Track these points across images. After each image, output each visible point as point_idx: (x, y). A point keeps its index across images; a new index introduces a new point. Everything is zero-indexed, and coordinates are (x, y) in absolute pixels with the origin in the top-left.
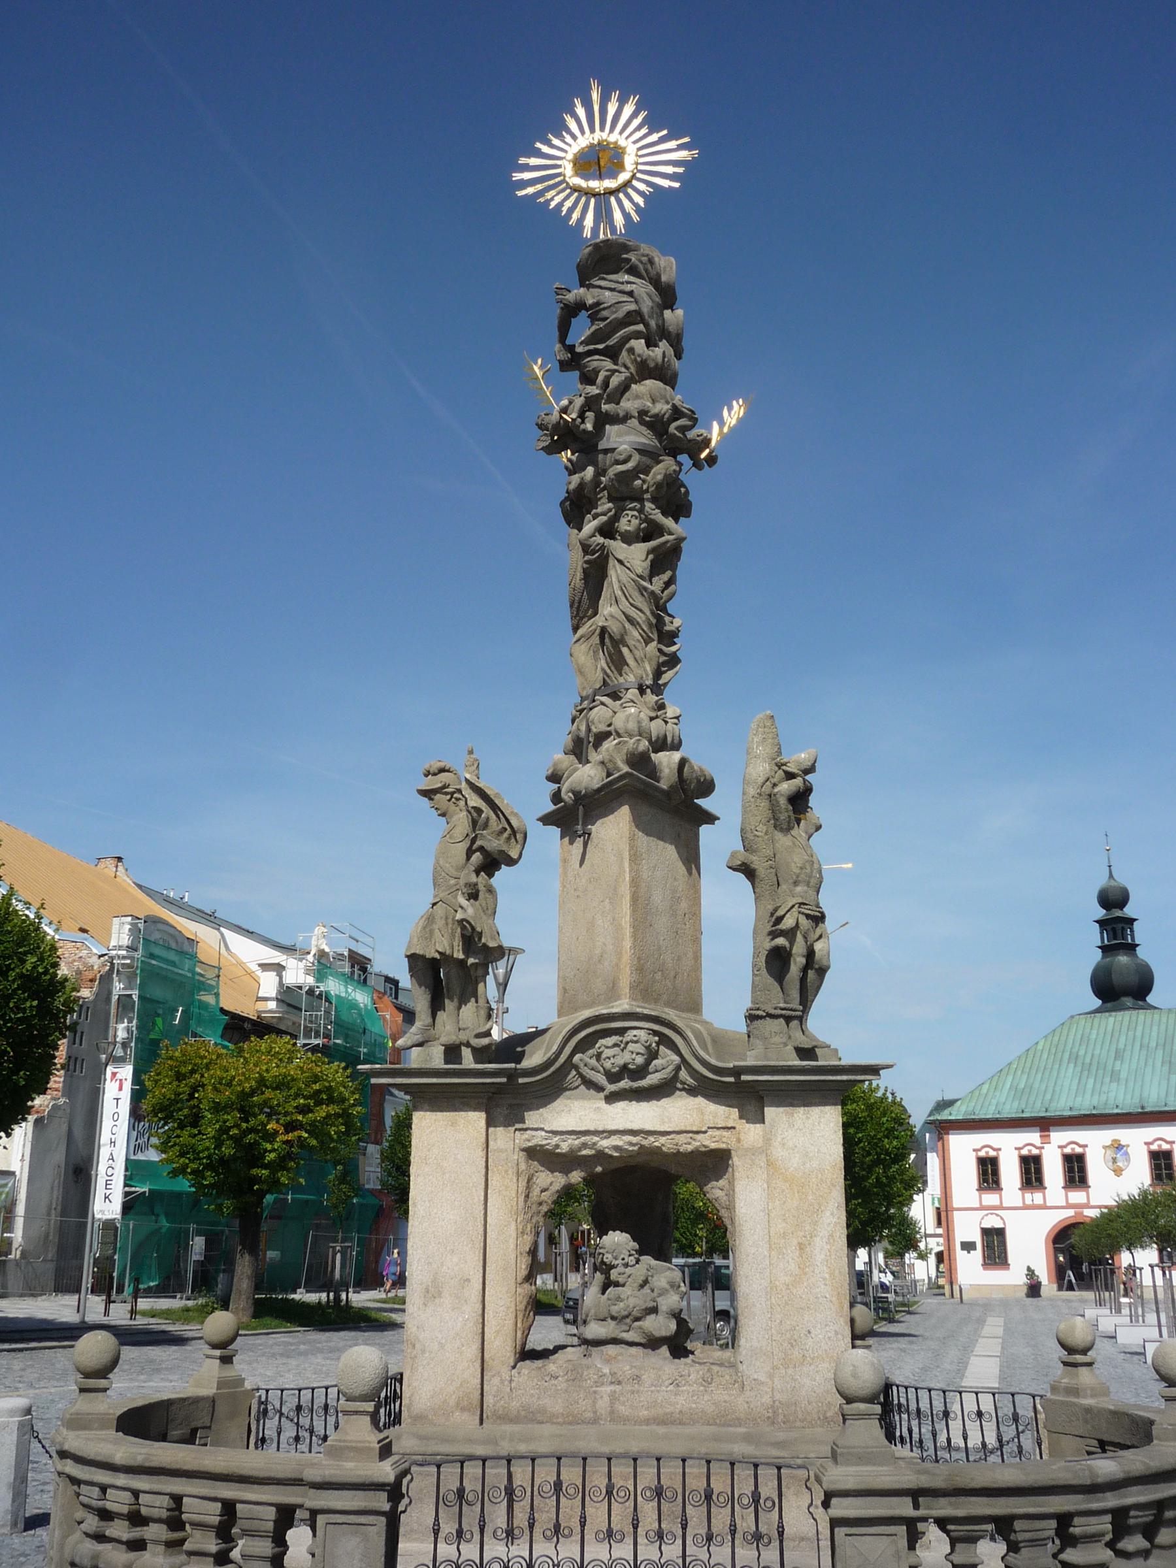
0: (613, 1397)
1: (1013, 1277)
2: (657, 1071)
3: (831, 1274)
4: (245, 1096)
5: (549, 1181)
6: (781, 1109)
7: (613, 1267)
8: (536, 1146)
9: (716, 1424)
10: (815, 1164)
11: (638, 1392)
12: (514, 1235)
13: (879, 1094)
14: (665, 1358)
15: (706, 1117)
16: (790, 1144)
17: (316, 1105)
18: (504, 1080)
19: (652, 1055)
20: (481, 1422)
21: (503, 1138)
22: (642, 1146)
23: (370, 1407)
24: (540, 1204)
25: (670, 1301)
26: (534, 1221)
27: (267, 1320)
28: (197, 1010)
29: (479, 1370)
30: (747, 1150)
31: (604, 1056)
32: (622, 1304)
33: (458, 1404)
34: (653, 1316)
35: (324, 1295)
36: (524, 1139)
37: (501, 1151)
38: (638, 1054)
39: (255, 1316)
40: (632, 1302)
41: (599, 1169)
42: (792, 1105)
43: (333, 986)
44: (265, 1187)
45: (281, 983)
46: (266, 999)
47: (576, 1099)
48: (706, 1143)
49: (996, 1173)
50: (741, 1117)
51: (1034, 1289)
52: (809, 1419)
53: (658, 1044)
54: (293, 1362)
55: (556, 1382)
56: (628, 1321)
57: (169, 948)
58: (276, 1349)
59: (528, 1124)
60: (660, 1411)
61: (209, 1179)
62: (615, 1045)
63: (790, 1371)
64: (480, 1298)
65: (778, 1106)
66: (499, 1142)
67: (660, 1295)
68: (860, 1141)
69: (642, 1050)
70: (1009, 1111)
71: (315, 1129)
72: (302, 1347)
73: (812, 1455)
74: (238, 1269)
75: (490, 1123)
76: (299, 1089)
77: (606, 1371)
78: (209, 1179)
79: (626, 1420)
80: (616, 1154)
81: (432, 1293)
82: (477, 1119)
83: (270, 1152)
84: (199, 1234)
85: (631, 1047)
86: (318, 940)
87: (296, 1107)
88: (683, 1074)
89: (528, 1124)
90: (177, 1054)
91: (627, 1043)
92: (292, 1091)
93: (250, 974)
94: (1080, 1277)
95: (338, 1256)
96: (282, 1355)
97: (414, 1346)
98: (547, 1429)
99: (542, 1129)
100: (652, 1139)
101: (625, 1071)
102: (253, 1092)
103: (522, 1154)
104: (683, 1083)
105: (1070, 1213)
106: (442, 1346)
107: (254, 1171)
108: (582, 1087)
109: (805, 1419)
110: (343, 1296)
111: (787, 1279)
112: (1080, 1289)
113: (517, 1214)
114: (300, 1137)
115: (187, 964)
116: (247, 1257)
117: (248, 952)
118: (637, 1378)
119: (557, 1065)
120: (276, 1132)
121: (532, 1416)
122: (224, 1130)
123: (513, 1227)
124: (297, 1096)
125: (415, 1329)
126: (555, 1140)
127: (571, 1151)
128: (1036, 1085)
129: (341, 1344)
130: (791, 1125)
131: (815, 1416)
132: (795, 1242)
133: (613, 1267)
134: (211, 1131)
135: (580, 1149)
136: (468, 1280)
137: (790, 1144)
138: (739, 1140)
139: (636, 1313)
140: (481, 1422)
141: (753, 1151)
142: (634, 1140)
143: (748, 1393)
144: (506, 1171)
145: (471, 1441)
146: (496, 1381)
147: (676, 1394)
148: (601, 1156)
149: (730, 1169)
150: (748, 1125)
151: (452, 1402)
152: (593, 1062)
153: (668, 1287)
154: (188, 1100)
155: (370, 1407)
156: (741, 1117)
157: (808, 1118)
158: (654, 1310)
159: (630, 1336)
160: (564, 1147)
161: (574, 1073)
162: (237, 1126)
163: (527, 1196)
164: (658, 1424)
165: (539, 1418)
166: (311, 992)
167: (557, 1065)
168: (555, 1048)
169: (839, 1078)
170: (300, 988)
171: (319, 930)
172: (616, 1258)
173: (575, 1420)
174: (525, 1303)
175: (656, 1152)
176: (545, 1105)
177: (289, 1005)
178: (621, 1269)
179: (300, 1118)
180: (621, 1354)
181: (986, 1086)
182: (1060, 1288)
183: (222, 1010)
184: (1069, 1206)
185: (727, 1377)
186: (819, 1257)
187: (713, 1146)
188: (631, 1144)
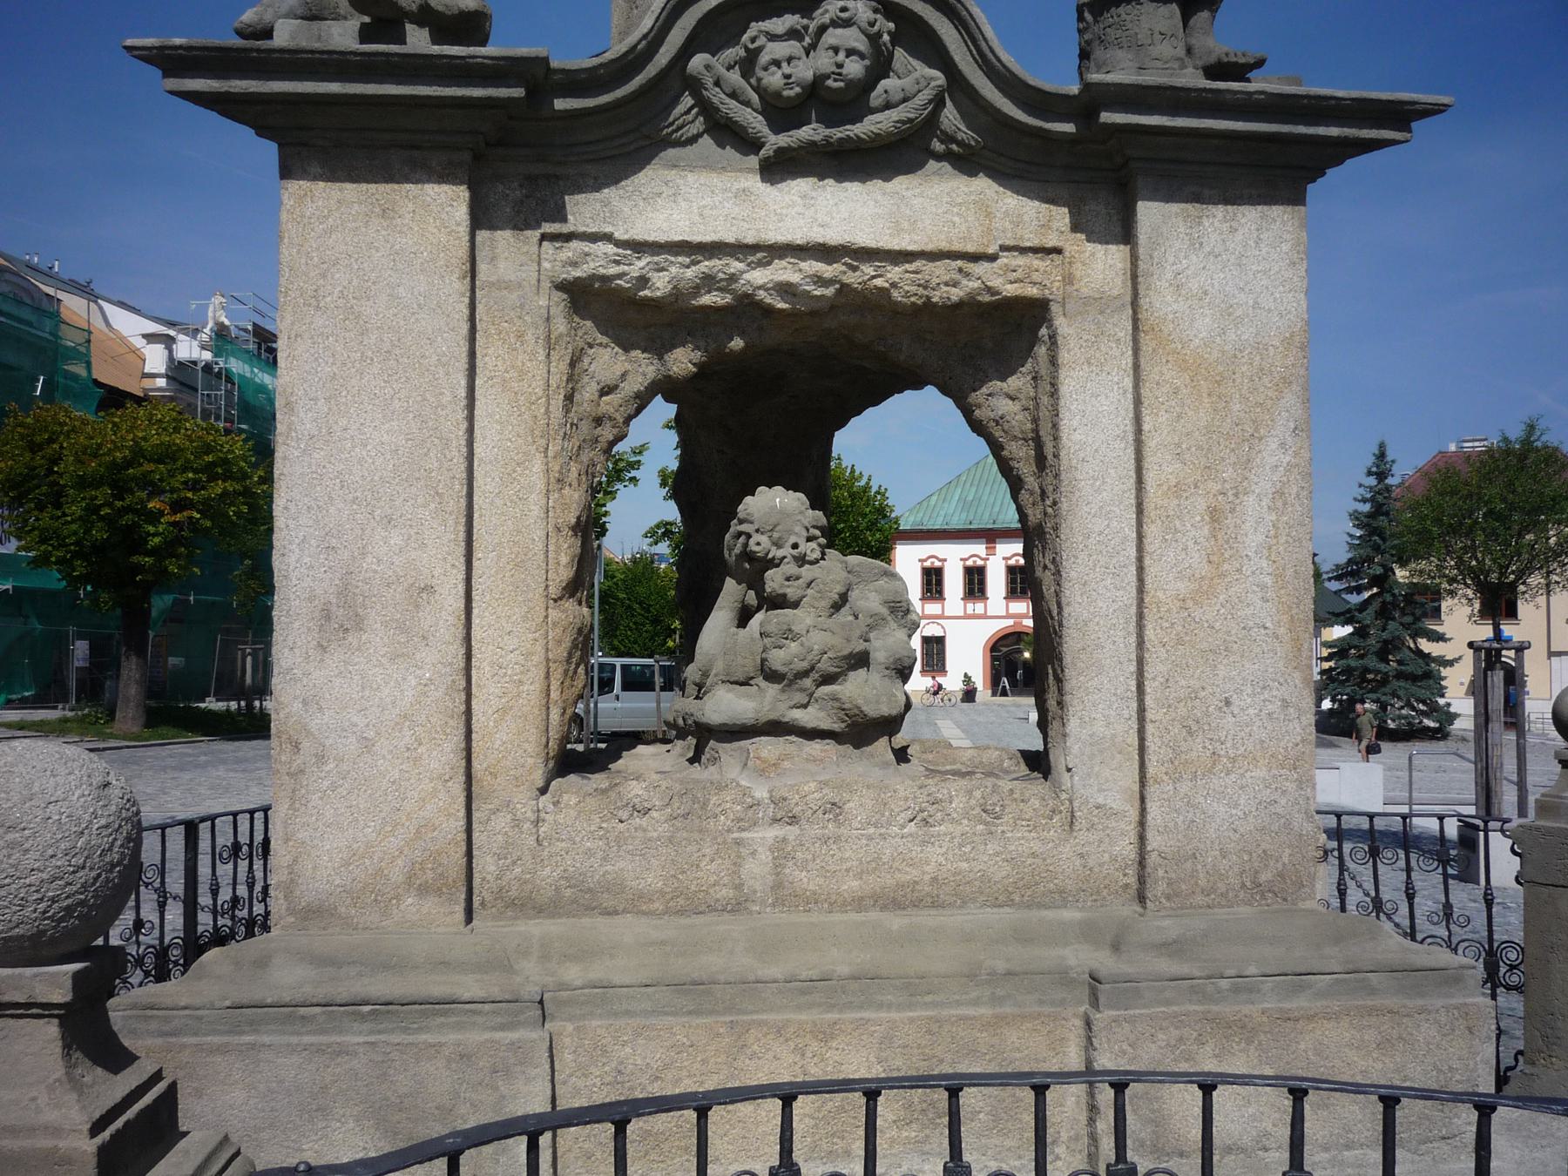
0: (781, 853)
1: (952, 682)
2: (888, 106)
3: (1278, 576)
4: (116, 467)
5: (618, 369)
6: (1175, 208)
7: (773, 563)
8: (593, 277)
9: (1010, 903)
10: (1247, 333)
11: (837, 839)
12: (540, 485)
13: (862, 483)
14: (886, 765)
15: (997, 224)
16: (1194, 285)
17: (209, 481)
18: (518, 92)
19: (881, 66)
20: (469, 918)
21: (514, 256)
22: (844, 288)
23: (55, 982)
24: (598, 421)
25: (891, 640)
26: (585, 457)
27: (163, 730)
28: (61, 380)
29: (462, 800)
30: (1087, 301)
31: (764, 58)
32: (794, 647)
33: (410, 878)
34: (861, 673)
35: (233, 705)
36: (560, 261)
37: (507, 286)
38: (850, 52)
39: (148, 725)
40: (817, 640)
41: (737, 343)
42: (1197, 199)
43: (236, 366)
44: (150, 578)
45: (171, 358)
46: (154, 376)
47: (692, 168)
48: (996, 283)
49: (940, 582)
50: (1075, 228)
51: (969, 695)
52: (1222, 887)
53: (896, 39)
54: (186, 776)
55: (644, 822)
56: (808, 682)
57: (20, 303)
58: (169, 761)
59: (574, 223)
60: (889, 881)
61: (80, 568)
62: (793, 34)
63: (1184, 787)
64: (461, 632)
65: (1169, 199)
66: (502, 265)
67: (871, 627)
68: (840, 532)
69: (861, 44)
70: (957, 523)
71: (206, 508)
72: (203, 758)
73: (1252, 970)
74: (124, 673)
75: (480, 218)
76: (188, 461)
77: (761, 793)
78: (80, 568)
79: (811, 901)
80: (781, 305)
81: (341, 621)
82: (446, 204)
83: (154, 535)
84: (81, 637)
85: (833, 36)
86: (217, 312)
87: (185, 483)
88: (950, 117)
89: (574, 223)
90: (29, 420)
91: (822, 29)
92: (179, 463)
93: (135, 351)
94: (1013, 683)
95: (249, 659)
96: (174, 768)
97: (297, 747)
98: (628, 928)
99: (608, 238)
100: (868, 270)
101: (818, 99)
102: (128, 463)
103: (559, 296)
104: (948, 138)
105: (1010, 622)
106: (367, 745)
107: (135, 559)
108: (706, 140)
109: (1213, 890)
110: (257, 703)
111: (1183, 587)
112: (1014, 694)
113: (546, 434)
114: (191, 518)
115: (48, 324)
116: (134, 659)
117: (130, 326)
118: (835, 808)
119: (651, 70)
120: (161, 513)
121: (588, 899)
122: (93, 510)
123: (538, 465)
124: (185, 470)
125: (297, 706)
126: (639, 265)
127: (677, 294)
128: (985, 498)
129: (251, 754)
130: (1196, 244)
131: (1234, 881)
132: (1201, 504)
133: (773, 563)
134: (75, 510)
135: (696, 291)
136: (429, 589)
137: (1194, 285)
138: (1069, 279)
139: (825, 666)
140: (469, 918)
141: (1099, 303)
142: (828, 270)
143: (1082, 836)
144: (520, 336)
145: (444, 965)
146: (502, 822)
147: (924, 843)
148: (747, 309)
149: (1041, 351)
150: (1090, 247)
151: (397, 874)
152: (735, 77)
153: (884, 611)
154: (47, 476)
155: (55, 982)
156: (1075, 228)
157: (1233, 230)
158: (860, 660)
159: (809, 717)
160: (661, 284)
161: (687, 101)
162: (108, 504)
163: (569, 398)
164: (884, 908)
165: (608, 901)
166: (208, 368)
167: (651, 70)
168: (647, 23)
169: (1321, 131)
170: (195, 363)
171: (217, 300)
172: (778, 544)
173: (688, 904)
174: (567, 644)
175: (875, 303)
176: (615, 180)
177: (182, 384)
178: (789, 568)
179: (190, 495)
180: (788, 757)
181: (934, 498)
182: (994, 694)
183: (95, 381)
184: (1008, 616)
185: (1036, 803)
186: (1253, 539)
187: (1010, 290)
188: (820, 281)
